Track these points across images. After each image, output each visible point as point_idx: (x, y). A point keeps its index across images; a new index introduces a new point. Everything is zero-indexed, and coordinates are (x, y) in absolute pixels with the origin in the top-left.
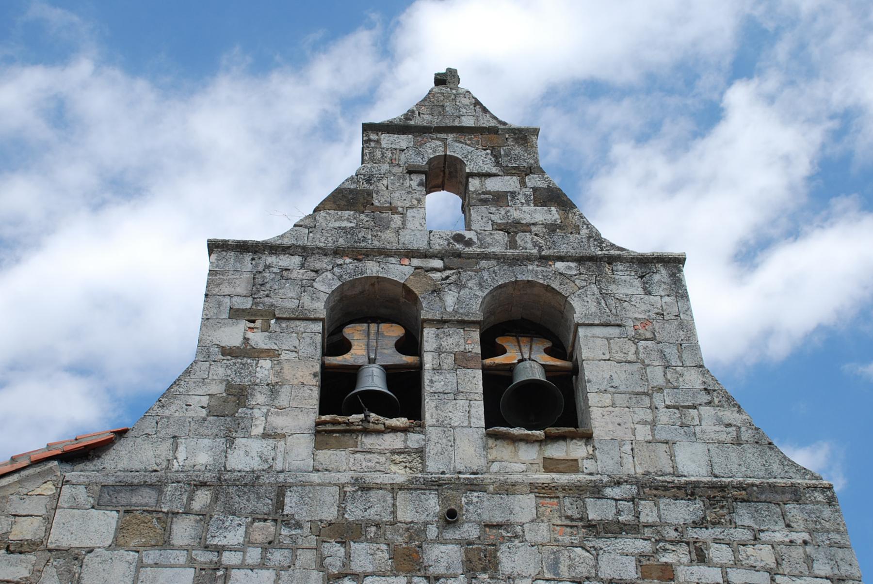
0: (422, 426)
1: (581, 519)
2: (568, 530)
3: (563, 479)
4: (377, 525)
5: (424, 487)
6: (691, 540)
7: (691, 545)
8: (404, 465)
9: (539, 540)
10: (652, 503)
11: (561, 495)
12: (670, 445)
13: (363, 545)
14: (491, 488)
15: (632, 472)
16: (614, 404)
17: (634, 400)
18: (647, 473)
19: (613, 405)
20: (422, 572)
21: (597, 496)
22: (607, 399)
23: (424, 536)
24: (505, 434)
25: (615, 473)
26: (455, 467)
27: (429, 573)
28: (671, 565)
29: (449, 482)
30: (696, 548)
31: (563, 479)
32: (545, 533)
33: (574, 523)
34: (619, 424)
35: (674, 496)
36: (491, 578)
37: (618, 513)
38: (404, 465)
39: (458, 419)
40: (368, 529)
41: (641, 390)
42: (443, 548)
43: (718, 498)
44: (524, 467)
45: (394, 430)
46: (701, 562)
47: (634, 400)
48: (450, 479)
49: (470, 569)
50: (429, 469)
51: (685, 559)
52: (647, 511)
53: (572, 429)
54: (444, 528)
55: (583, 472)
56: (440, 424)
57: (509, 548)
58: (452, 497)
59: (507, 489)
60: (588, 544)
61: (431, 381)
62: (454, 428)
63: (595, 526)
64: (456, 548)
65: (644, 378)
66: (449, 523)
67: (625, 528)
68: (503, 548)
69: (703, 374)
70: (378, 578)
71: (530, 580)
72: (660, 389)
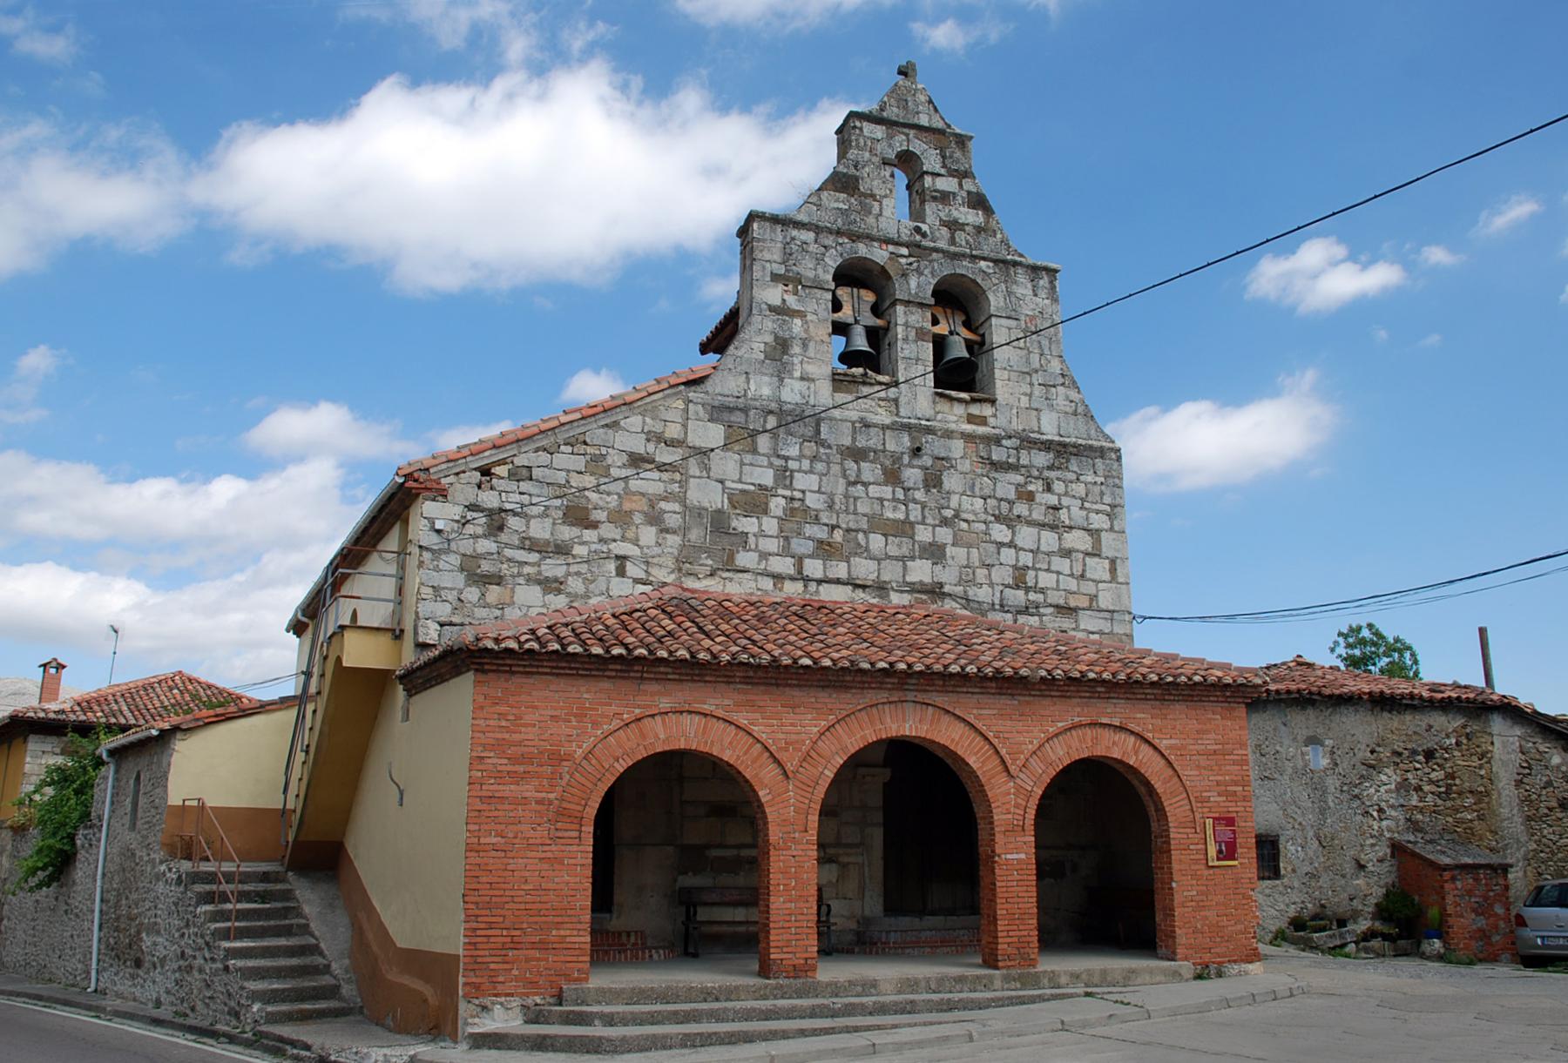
59: (949, 434)
65: (1028, 362)
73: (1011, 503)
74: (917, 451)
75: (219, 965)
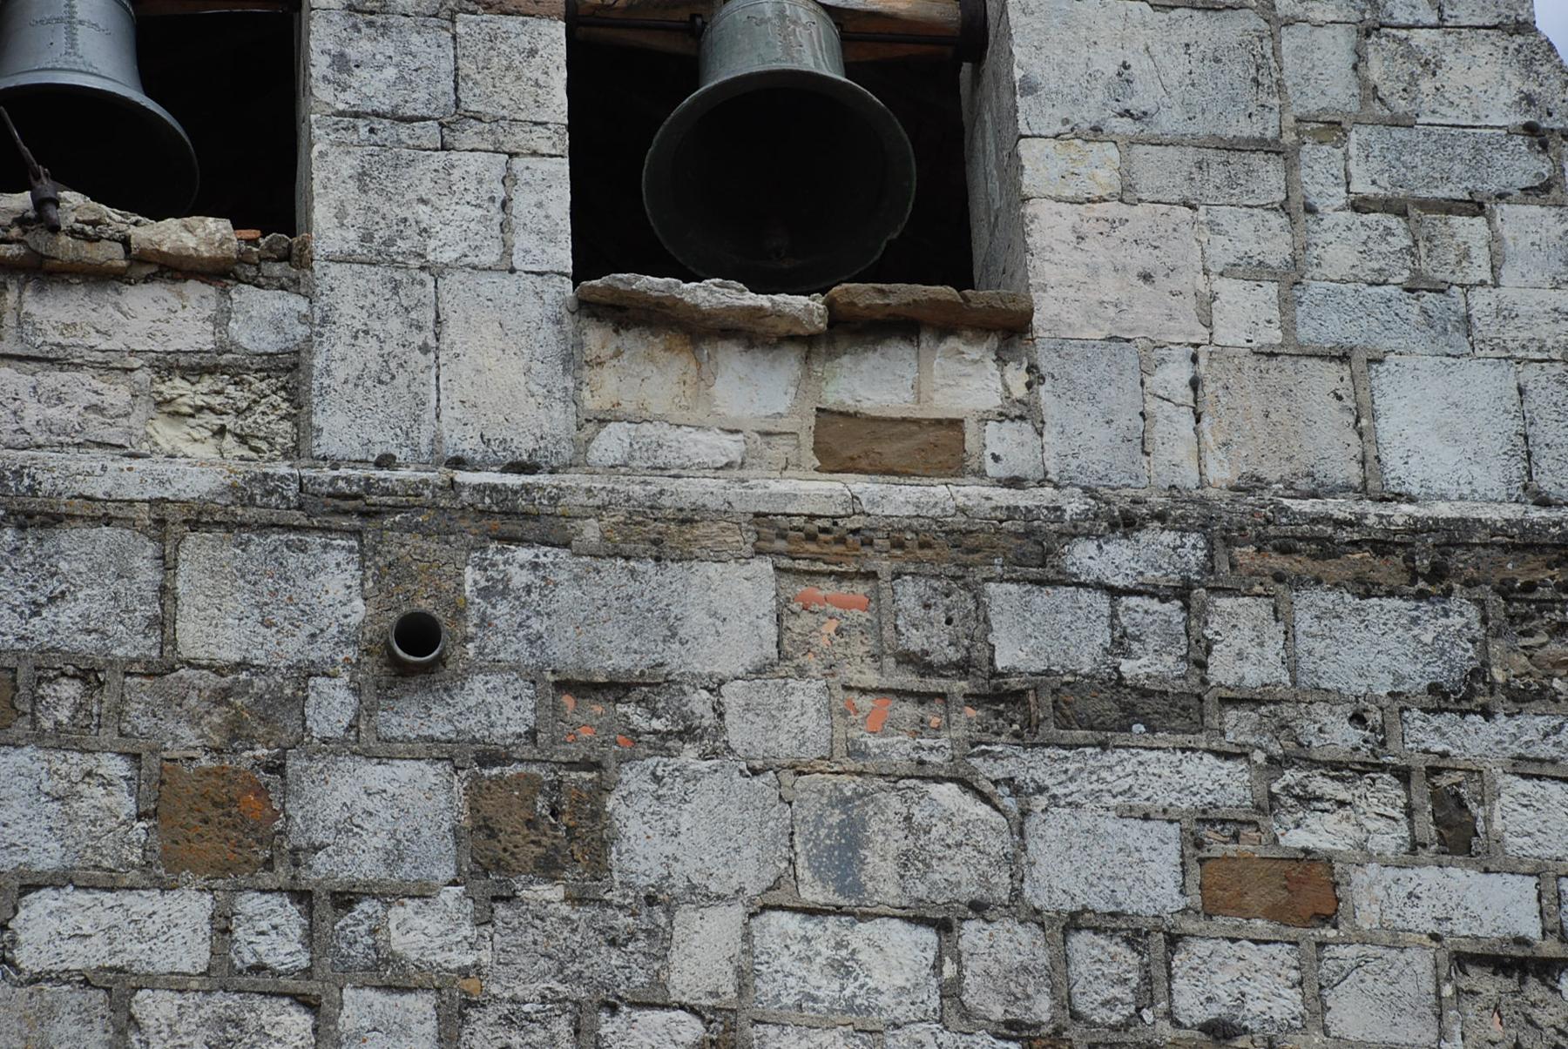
0: (298, 258)
1: (963, 668)
2: (909, 709)
3: (896, 499)
4: (89, 676)
5: (299, 518)
6: (1419, 762)
7: (1417, 782)
8: (216, 421)
9: (785, 745)
10: (1262, 609)
11: (884, 566)
12: (1358, 364)
13: (21, 758)
14: (591, 531)
15: (1188, 478)
16: (1128, 187)
17: (1217, 175)
18: (1251, 485)
19: (1126, 194)
20: (282, 874)
21: (1034, 572)
22: (1100, 167)
23: (293, 723)
24: (659, 304)
25: (1117, 479)
26: (437, 439)
27: (308, 879)
28: (1328, 860)
29: (410, 502)
30: (1437, 796)
31: (896, 499)
32: (812, 722)
33: (933, 684)
34: (1146, 277)
35: (1359, 580)
36: (577, 899)
37: (1121, 644)
38: (216, 421)
39: (454, 228)
40: (46, 690)
41: (1249, 129)
42: (375, 774)
43: (1545, 593)
44: (732, 447)
45: (172, 269)
46: (1454, 851)
47: (1217, 175)
48: (416, 489)
49: (491, 865)
50: (327, 444)
51: (1389, 839)
52: (1241, 638)
53: (945, 292)
54: (384, 691)
55: (981, 473)
56: (376, 254)
57: (657, 779)
58: (423, 560)
59: (660, 535)
60: (986, 770)
61: (341, 62)
62: (438, 272)
63: (1018, 696)
64: (431, 774)
65: (1265, 76)
66: (404, 671)
67: (1146, 707)
68: (633, 778)
69: (1528, 64)
70: (83, 898)
71: (737, 912)
72: (1333, 128)
73: (1154, 942)
74: (415, 648)
75: (1401, 86)
